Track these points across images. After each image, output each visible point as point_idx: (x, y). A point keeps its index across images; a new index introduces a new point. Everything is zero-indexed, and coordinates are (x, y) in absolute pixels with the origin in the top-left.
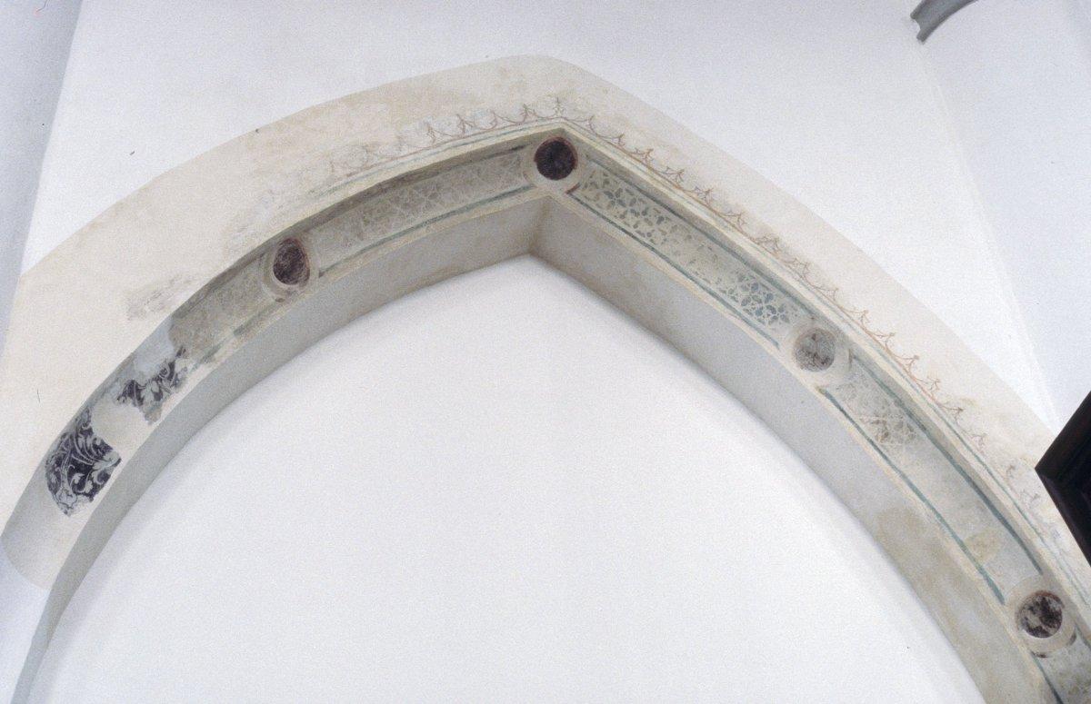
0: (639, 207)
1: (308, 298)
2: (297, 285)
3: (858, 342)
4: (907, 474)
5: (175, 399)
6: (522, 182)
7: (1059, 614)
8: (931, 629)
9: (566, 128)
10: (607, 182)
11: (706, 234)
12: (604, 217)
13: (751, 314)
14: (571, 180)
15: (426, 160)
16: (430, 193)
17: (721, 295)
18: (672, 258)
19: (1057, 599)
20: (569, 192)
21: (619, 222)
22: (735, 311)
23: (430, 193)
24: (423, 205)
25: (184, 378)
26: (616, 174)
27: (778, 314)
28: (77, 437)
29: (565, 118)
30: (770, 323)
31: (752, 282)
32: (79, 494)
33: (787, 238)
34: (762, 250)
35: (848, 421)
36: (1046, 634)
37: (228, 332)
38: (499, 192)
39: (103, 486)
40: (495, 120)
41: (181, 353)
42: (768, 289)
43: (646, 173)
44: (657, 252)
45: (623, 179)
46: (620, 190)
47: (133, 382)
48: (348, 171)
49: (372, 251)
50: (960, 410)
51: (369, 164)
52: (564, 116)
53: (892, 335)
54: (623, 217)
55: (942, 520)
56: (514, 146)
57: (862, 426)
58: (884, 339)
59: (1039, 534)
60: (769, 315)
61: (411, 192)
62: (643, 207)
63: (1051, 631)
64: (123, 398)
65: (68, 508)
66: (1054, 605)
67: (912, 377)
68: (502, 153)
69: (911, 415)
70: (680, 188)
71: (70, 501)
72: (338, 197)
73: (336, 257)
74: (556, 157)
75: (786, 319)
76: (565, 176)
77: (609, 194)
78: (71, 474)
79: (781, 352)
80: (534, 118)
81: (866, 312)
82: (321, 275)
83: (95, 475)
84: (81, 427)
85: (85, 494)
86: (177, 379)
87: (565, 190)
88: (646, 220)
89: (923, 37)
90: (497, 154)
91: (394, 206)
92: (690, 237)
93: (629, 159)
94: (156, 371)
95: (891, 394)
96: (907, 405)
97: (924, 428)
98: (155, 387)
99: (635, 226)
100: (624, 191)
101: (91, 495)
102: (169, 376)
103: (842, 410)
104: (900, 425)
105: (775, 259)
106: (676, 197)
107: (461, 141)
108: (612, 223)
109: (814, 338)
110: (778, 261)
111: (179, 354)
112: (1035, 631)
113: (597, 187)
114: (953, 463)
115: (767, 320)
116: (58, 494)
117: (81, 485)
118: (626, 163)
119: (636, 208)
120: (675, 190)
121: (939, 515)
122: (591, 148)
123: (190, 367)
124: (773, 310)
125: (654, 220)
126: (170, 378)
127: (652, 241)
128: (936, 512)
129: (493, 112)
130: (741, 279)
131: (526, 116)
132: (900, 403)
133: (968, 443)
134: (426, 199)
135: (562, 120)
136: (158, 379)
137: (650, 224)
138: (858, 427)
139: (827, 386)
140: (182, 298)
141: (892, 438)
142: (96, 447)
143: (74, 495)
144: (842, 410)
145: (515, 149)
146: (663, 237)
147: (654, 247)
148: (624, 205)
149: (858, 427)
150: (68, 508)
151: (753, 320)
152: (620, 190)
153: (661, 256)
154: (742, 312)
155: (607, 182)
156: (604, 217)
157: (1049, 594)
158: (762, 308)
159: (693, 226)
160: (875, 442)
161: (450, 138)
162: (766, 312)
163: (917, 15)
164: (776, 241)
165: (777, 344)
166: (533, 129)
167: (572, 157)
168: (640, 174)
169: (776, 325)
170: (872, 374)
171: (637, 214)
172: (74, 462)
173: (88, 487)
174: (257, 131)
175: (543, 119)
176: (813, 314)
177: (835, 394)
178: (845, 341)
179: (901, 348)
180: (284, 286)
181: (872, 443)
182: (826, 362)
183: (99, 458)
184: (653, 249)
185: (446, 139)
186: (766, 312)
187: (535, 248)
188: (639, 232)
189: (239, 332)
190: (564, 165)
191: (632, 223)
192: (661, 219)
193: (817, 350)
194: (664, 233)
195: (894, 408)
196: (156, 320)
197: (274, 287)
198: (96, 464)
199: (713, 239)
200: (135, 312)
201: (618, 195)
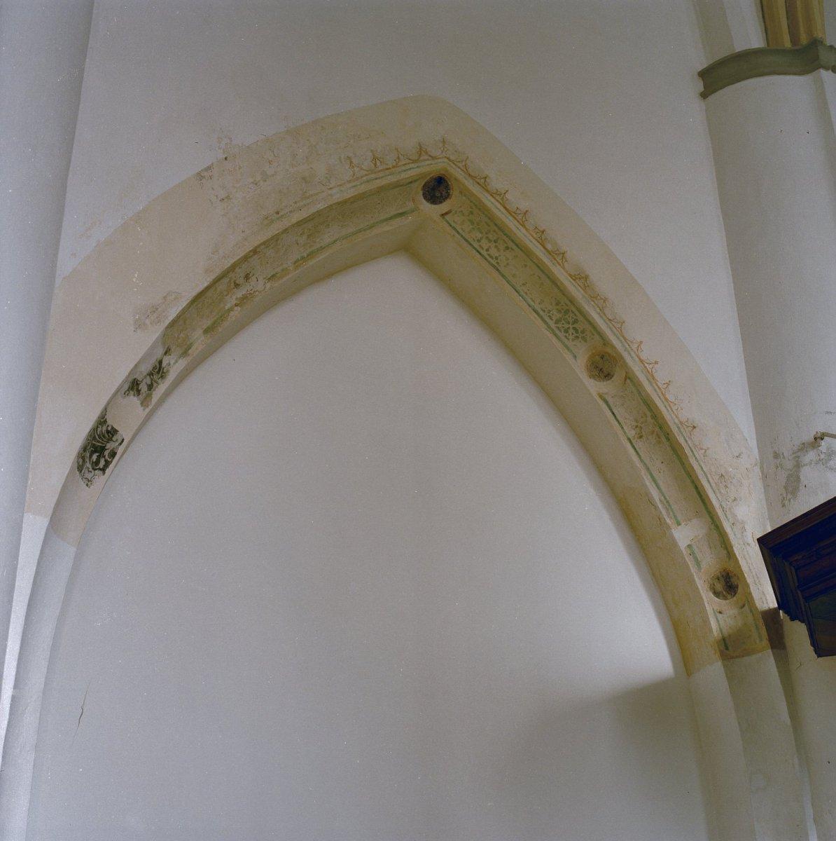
3: (633, 368)
6: (411, 205)
8: (652, 598)
9: (448, 168)
10: (472, 213)
13: (560, 331)
14: (444, 207)
17: (541, 313)
20: (443, 215)
21: (476, 245)
22: (549, 327)
25: (168, 371)
27: (580, 335)
30: (573, 340)
32: (96, 469)
34: (577, 285)
35: (616, 423)
37: (199, 332)
38: (393, 213)
39: (111, 462)
40: (398, 158)
42: (575, 315)
44: (500, 272)
50: (694, 427)
52: (448, 156)
53: (656, 363)
54: (479, 241)
58: (651, 366)
63: (729, 596)
64: (128, 392)
65: (89, 481)
66: (734, 580)
67: (666, 399)
69: (661, 428)
71: (89, 476)
75: (584, 339)
76: (441, 202)
79: (578, 365)
80: (426, 157)
81: (641, 342)
83: (106, 453)
84: (102, 421)
85: (100, 469)
86: (163, 372)
88: (496, 247)
92: (526, 266)
93: (490, 198)
95: (651, 410)
97: (668, 439)
98: (148, 380)
99: (487, 250)
101: (103, 470)
102: (159, 371)
103: (613, 414)
105: (584, 294)
106: (521, 234)
107: (373, 176)
110: (586, 296)
111: (166, 353)
113: (463, 215)
114: (684, 468)
115: (571, 337)
116: (83, 472)
117: (97, 463)
119: (490, 236)
123: (172, 363)
124: (576, 330)
126: (158, 372)
127: (498, 263)
129: (397, 149)
130: (557, 304)
131: (420, 155)
133: (695, 453)
135: (446, 160)
136: (150, 374)
137: (499, 250)
139: (606, 394)
140: (173, 313)
142: (108, 432)
143: (93, 471)
144: (613, 414)
148: (481, 233)
150: (89, 481)
151: (561, 335)
158: (569, 328)
162: (571, 331)
163: (703, 74)
164: (587, 277)
165: (575, 357)
170: (639, 393)
171: (490, 241)
172: (94, 446)
175: (433, 158)
176: (606, 342)
178: (625, 365)
179: (661, 376)
182: (608, 376)
183: (110, 440)
184: (498, 270)
186: (571, 331)
187: (408, 249)
188: (489, 255)
190: (441, 194)
192: (507, 248)
193: (605, 365)
195: (649, 419)
196: (154, 333)
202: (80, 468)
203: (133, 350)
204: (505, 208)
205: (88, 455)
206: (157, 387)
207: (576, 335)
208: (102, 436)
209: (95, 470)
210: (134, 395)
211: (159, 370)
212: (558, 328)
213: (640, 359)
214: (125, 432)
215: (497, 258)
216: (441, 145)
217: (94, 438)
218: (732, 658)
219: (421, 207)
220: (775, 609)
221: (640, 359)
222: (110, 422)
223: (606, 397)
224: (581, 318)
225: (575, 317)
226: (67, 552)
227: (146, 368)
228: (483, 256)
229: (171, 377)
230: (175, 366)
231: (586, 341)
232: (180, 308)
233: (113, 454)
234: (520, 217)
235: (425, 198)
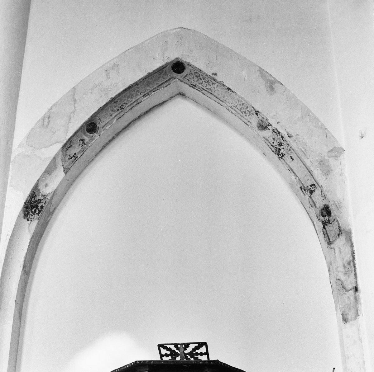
0: (206, 80)
1: (98, 139)
6: (169, 77)
16: (136, 91)
23: (136, 91)
24: (135, 95)
28: (31, 199)
60: (248, 113)
73: (106, 121)
78: (31, 210)
83: (39, 208)
85: (36, 214)
88: (209, 84)
117: (35, 211)
125: (211, 84)
127: (211, 91)
134: (135, 93)
147: (212, 93)
148: (201, 80)
150: (32, 219)
151: (243, 115)
158: (246, 111)
162: (247, 112)
172: (32, 206)
173: (37, 211)
180: (91, 135)
183: (40, 202)
188: (207, 89)
191: (205, 86)
192: (213, 84)
197: (87, 136)
198: (39, 204)
201: (199, 77)
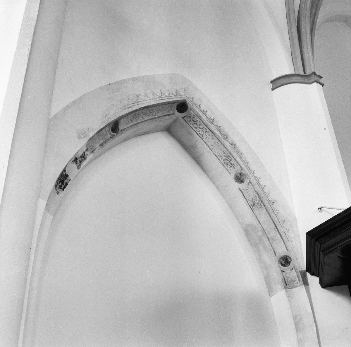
0: (201, 127)
2: (115, 134)
4: (257, 217)
5: (84, 163)
6: (172, 112)
7: (290, 262)
9: (187, 100)
11: (218, 139)
12: (191, 127)
13: (225, 164)
14: (184, 114)
15: (152, 103)
17: (218, 156)
18: (207, 143)
19: (290, 258)
20: (183, 117)
21: (195, 130)
24: (148, 115)
26: (197, 116)
27: (232, 166)
29: (186, 97)
30: (230, 167)
31: (227, 155)
33: (238, 145)
36: (285, 266)
37: (98, 145)
38: (166, 114)
39: (66, 187)
41: (87, 150)
43: (205, 118)
45: (199, 118)
46: (197, 121)
47: (76, 157)
48: (133, 102)
49: (133, 126)
50: (274, 203)
51: (138, 101)
53: (260, 178)
54: (196, 128)
55: (264, 231)
56: (173, 102)
57: (248, 201)
59: (288, 240)
61: (146, 111)
62: (202, 127)
63: (287, 266)
66: (289, 259)
67: (264, 191)
68: (170, 104)
69: (262, 202)
70: (213, 124)
71: (58, 190)
72: (130, 110)
73: (126, 127)
74: (182, 107)
76: (183, 113)
77: (194, 121)
80: (179, 95)
82: (121, 131)
83: (64, 183)
84: (64, 171)
87: (182, 116)
88: (202, 131)
89: (273, 89)
90: (169, 104)
91: (141, 114)
93: (202, 113)
94: (81, 154)
95: (258, 195)
96: (261, 199)
97: (264, 206)
100: (198, 121)
101: (63, 189)
102: (83, 157)
104: (258, 203)
106: (212, 127)
108: (193, 129)
109: (240, 174)
111: (87, 150)
112: (283, 265)
117: (61, 186)
118: (201, 114)
119: (200, 127)
120: (212, 125)
121: (264, 229)
122: (192, 107)
123: (88, 154)
125: (204, 131)
126: (83, 157)
127: (203, 137)
128: (263, 228)
132: (260, 198)
135: (186, 97)
136: (81, 157)
137: (203, 132)
138: (247, 201)
140: (91, 135)
141: (255, 206)
142: (66, 175)
145: (173, 103)
146: (206, 137)
148: (197, 125)
149: (247, 201)
151: (225, 165)
152: (197, 121)
153: (204, 141)
154: (223, 163)
155: (194, 117)
156: (191, 127)
157: (288, 256)
159: (215, 136)
160: (251, 206)
161: (158, 97)
164: (235, 145)
165: (230, 174)
166: (179, 98)
167: (186, 108)
168: (204, 117)
169: (231, 168)
171: (200, 128)
174: (110, 84)
175: (181, 96)
177: (243, 191)
180: (112, 133)
181: (250, 206)
182: (242, 182)
183: (66, 179)
184: (202, 139)
185: (157, 97)
186: (229, 164)
187: (169, 130)
188: (199, 133)
189: (100, 145)
192: (206, 132)
194: (206, 136)
195: (257, 198)
196: (85, 141)
199: (219, 141)
200: (79, 137)
201: (196, 122)
202: (56, 186)
203: (77, 146)
204: (206, 116)
205: (59, 182)
206: (83, 162)
207: (231, 165)
208: (63, 176)
209: (60, 189)
210: (75, 164)
211: (84, 156)
212: (224, 162)
213: (254, 176)
214: (71, 177)
215: (202, 135)
216: (184, 92)
217: (61, 176)
218: (288, 289)
219: (176, 113)
220: (304, 271)
221: (254, 176)
222: (67, 171)
223: (241, 189)
224: (233, 159)
225: (231, 159)
226: (50, 217)
227: (80, 154)
228: (197, 134)
229: (88, 159)
230: (90, 157)
231: (234, 168)
232: (94, 134)
233: (67, 184)
234: (212, 120)
235: (177, 107)
